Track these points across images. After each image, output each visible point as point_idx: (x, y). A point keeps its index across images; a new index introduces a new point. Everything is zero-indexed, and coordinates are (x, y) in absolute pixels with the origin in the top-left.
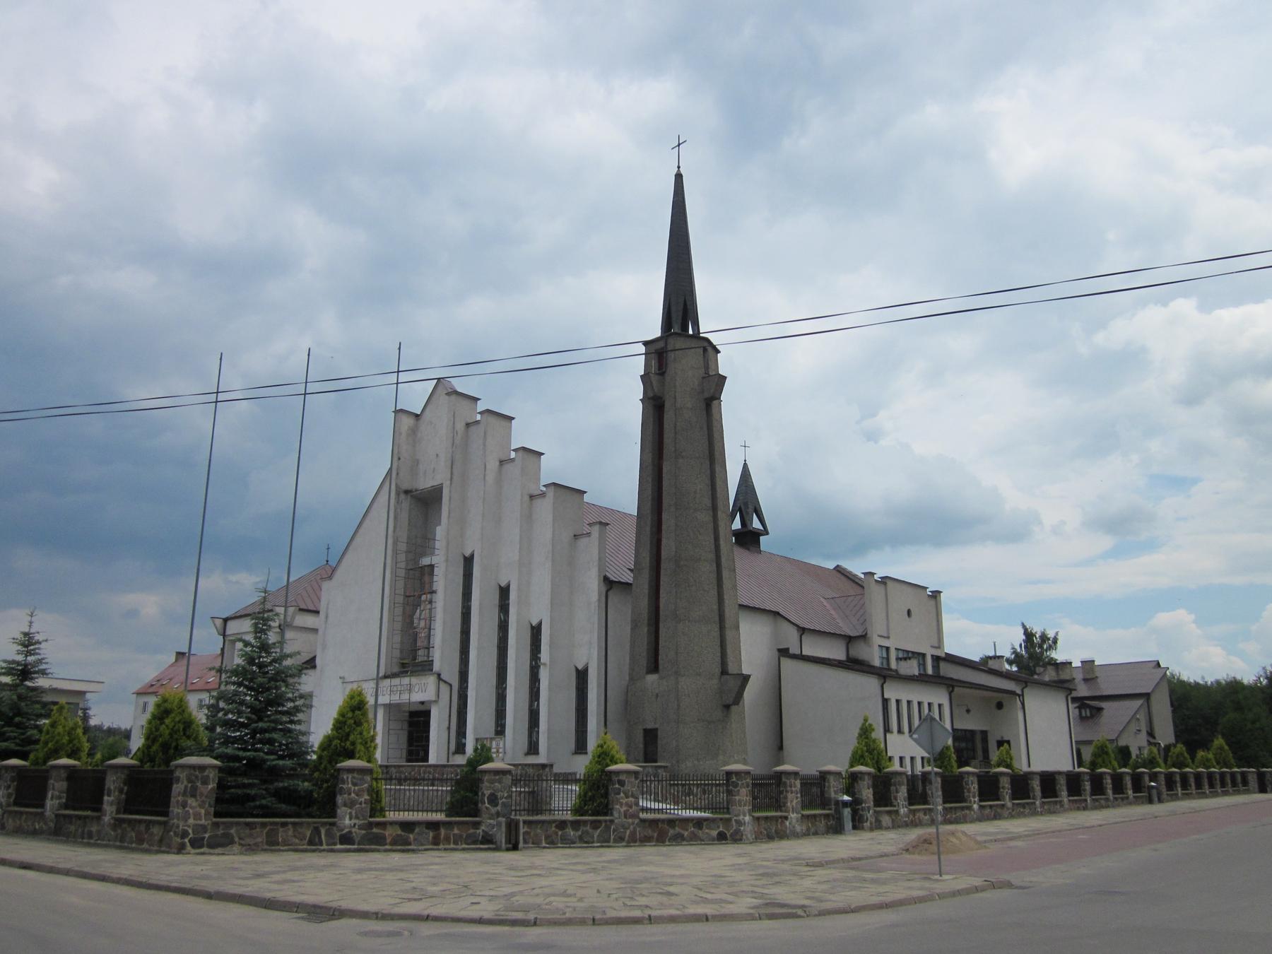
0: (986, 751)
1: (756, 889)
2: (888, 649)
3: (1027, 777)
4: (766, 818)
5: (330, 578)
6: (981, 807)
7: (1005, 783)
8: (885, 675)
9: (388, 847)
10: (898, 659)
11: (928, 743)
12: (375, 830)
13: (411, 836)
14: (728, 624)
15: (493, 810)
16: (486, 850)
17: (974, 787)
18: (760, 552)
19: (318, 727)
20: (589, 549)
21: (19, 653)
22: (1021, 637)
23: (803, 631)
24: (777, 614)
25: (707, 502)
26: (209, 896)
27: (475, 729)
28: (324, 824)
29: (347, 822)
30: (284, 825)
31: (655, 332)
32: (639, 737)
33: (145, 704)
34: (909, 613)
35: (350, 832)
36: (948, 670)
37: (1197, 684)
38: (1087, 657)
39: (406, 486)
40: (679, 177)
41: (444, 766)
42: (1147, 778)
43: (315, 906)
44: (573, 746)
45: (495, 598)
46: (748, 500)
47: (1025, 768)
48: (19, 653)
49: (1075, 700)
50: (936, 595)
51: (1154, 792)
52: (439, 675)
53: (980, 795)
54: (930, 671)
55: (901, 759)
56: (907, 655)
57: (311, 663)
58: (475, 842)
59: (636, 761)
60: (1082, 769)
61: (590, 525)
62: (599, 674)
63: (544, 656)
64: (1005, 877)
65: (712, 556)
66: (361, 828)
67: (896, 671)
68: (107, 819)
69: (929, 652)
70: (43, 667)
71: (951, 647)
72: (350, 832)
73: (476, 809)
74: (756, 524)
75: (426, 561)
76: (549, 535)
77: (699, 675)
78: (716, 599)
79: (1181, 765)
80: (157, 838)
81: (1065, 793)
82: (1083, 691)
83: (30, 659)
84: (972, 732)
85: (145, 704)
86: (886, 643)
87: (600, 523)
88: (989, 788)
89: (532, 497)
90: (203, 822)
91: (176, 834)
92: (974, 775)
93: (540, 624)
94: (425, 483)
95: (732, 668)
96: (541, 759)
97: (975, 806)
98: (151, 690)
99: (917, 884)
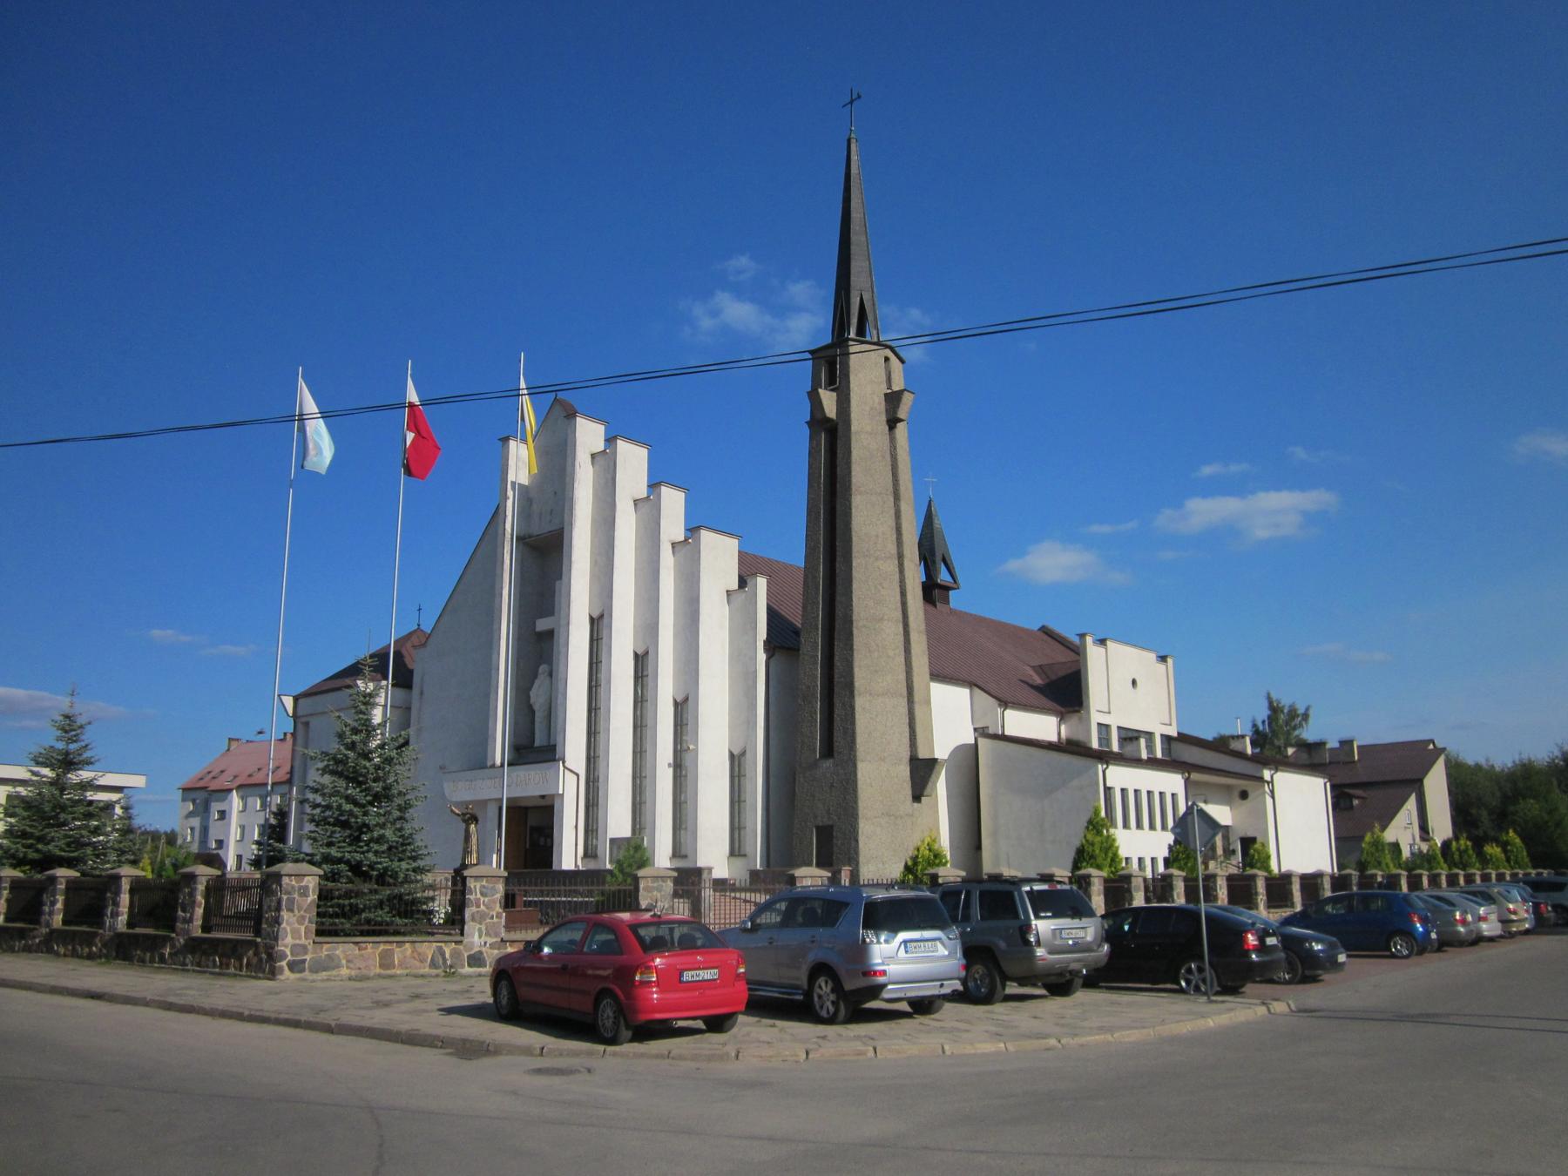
2: (1107, 726)
3: (1286, 878)
7: (1261, 886)
14: (917, 697)
21: (59, 739)
22: (1262, 713)
25: (893, 549)
26: (329, 1029)
34: (1134, 682)
35: (480, 952)
37: (1478, 767)
38: (1345, 736)
43: (464, 1041)
48: (59, 739)
54: (1159, 755)
64: (358, 985)
65: (899, 614)
66: (492, 946)
70: (87, 755)
72: (480, 952)
75: (542, 625)
77: (883, 759)
78: (903, 667)
83: (73, 747)
86: (1105, 720)
90: (303, 941)
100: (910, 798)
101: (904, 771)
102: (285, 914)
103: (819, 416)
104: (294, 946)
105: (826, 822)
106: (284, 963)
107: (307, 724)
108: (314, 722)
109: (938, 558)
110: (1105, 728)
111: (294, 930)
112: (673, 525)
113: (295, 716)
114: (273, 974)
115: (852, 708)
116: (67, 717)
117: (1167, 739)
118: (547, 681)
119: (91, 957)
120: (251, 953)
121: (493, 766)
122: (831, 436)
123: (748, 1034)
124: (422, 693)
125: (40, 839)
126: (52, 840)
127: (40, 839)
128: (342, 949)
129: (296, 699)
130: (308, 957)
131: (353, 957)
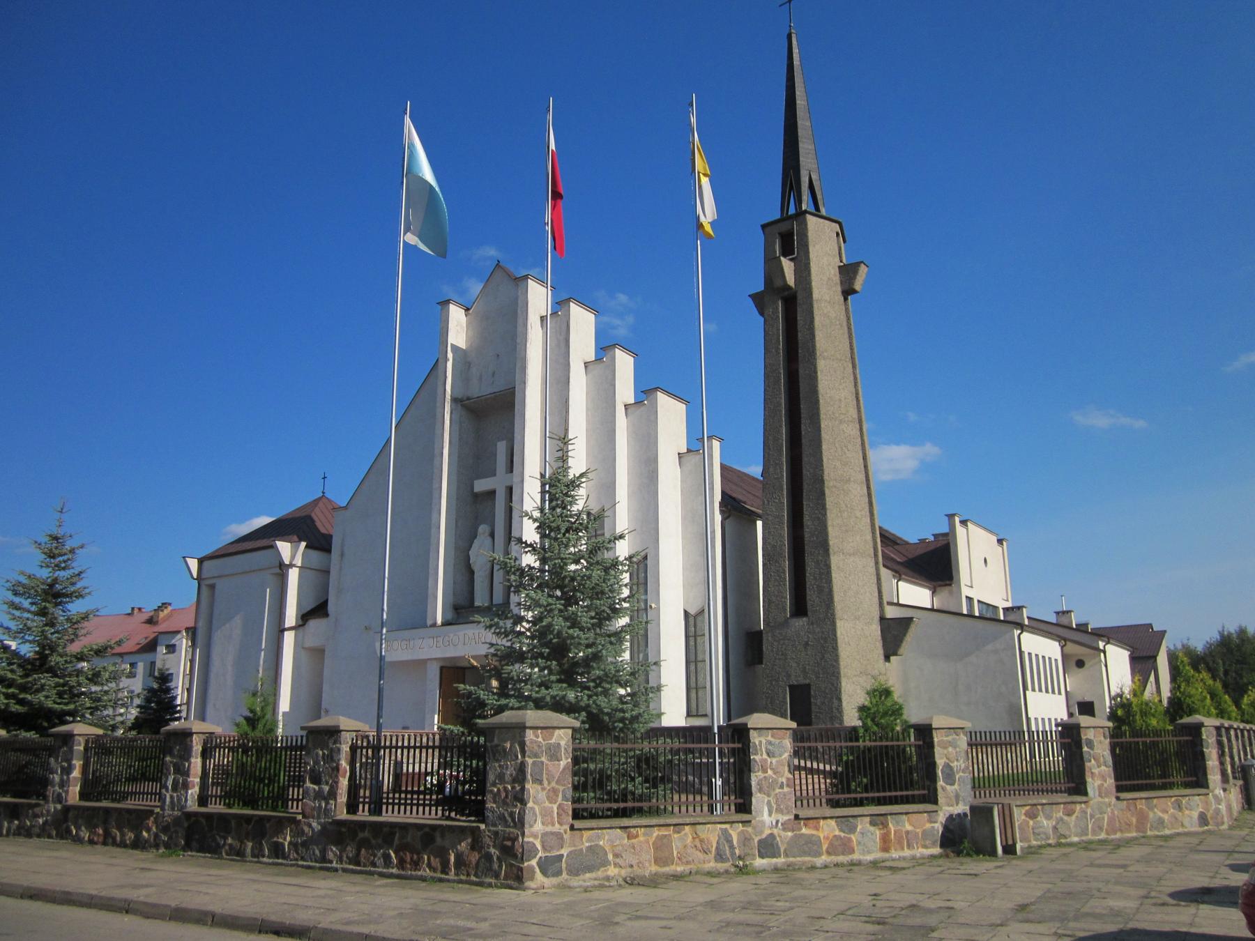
35: (772, 835)
66: (786, 826)
72: (772, 835)
100: (882, 657)
101: (876, 629)
102: (530, 787)
103: (778, 283)
104: (545, 834)
105: (802, 681)
106: (534, 862)
107: (212, 587)
108: (221, 585)
110: (969, 599)
111: (545, 813)
112: (625, 391)
113: (199, 579)
114: (517, 878)
115: (828, 567)
116: (56, 538)
117: (1006, 610)
118: (489, 540)
119: (138, 844)
120: (463, 846)
121: (434, 625)
122: (786, 309)
124: (342, 555)
125: (24, 688)
126: (42, 688)
127: (24, 688)
128: (607, 837)
129: (201, 561)
130: (564, 852)
131: (624, 846)
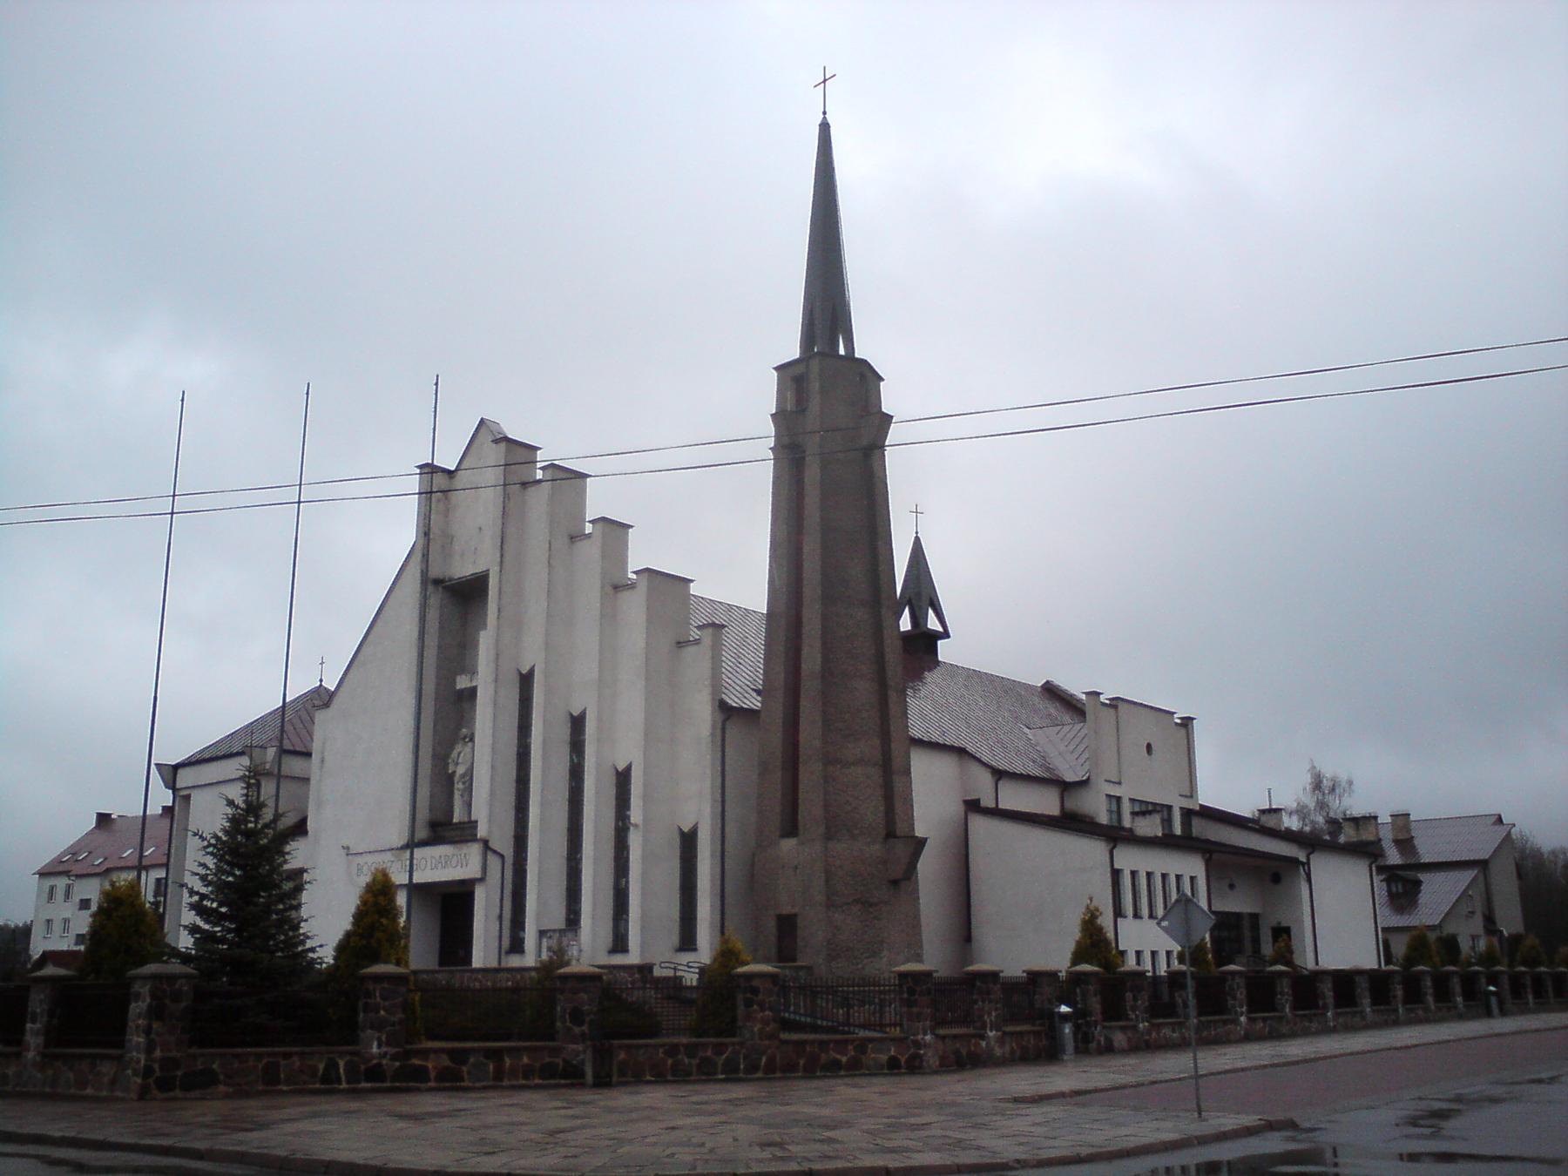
0: (1256, 941)
1: (949, 1133)
2: (1119, 799)
4: (955, 1037)
5: (327, 705)
6: (1249, 1019)
7: (1285, 986)
8: (1115, 836)
9: (432, 1084)
10: (1134, 814)
11: (1182, 931)
12: (416, 1062)
13: (464, 1069)
15: (577, 1030)
16: (566, 1086)
17: (1241, 994)
18: (938, 663)
19: (325, 921)
20: (696, 663)
23: (999, 774)
24: (961, 752)
27: (539, 916)
28: (341, 1054)
29: (375, 1050)
30: (287, 1056)
31: (794, 352)
32: (771, 925)
33: (52, 888)
34: (1149, 746)
35: (380, 1065)
36: (1200, 828)
38: (1401, 809)
39: (435, 572)
40: (825, 128)
41: (497, 970)
42: (1483, 980)
44: (675, 939)
45: (564, 732)
46: (922, 592)
47: (1311, 965)
49: (1381, 869)
50: (1187, 722)
51: (1494, 1000)
52: (486, 843)
53: (1249, 1006)
54: (1178, 830)
55: (1138, 953)
56: (1145, 809)
57: (300, 829)
58: (552, 1077)
59: (766, 960)
60: (1391, 967)
61: (699, 628)
62: (713, 835)
63: (636, 814)
66: (394, 1058)
67: (1131, 830)
68: (31, 1055)
69: (1178, 804)
71: (1210, 794)
72: (380, 1065)
73: (590, 1031)
74: (933, 623)
75: (462, 683)
76: (641, 643)
79: (1532, 962)
80: (106, 1079)
81: (1366, 1001)
82: (1393, 857)
84: (1238, 916)
85: (52, 888)
87: (713, 625)
88: (1262, 994)
89: (616, 588)
90: (174, 1054)
91: (135, 1073)
92: (1242, 979)
93: (629, 768)
94: (462, 569)
95: (901, 828)
96: (633, 957)
97: (1243, 1019)
98: (61, 869)
99: (1169, 1124)
107: (188, 798)
109: (925, 600)
123: (673, 1155)
